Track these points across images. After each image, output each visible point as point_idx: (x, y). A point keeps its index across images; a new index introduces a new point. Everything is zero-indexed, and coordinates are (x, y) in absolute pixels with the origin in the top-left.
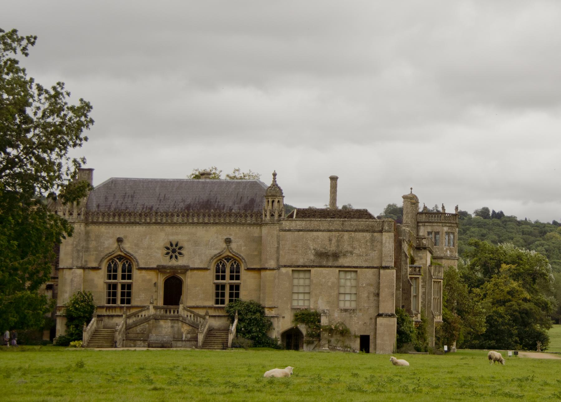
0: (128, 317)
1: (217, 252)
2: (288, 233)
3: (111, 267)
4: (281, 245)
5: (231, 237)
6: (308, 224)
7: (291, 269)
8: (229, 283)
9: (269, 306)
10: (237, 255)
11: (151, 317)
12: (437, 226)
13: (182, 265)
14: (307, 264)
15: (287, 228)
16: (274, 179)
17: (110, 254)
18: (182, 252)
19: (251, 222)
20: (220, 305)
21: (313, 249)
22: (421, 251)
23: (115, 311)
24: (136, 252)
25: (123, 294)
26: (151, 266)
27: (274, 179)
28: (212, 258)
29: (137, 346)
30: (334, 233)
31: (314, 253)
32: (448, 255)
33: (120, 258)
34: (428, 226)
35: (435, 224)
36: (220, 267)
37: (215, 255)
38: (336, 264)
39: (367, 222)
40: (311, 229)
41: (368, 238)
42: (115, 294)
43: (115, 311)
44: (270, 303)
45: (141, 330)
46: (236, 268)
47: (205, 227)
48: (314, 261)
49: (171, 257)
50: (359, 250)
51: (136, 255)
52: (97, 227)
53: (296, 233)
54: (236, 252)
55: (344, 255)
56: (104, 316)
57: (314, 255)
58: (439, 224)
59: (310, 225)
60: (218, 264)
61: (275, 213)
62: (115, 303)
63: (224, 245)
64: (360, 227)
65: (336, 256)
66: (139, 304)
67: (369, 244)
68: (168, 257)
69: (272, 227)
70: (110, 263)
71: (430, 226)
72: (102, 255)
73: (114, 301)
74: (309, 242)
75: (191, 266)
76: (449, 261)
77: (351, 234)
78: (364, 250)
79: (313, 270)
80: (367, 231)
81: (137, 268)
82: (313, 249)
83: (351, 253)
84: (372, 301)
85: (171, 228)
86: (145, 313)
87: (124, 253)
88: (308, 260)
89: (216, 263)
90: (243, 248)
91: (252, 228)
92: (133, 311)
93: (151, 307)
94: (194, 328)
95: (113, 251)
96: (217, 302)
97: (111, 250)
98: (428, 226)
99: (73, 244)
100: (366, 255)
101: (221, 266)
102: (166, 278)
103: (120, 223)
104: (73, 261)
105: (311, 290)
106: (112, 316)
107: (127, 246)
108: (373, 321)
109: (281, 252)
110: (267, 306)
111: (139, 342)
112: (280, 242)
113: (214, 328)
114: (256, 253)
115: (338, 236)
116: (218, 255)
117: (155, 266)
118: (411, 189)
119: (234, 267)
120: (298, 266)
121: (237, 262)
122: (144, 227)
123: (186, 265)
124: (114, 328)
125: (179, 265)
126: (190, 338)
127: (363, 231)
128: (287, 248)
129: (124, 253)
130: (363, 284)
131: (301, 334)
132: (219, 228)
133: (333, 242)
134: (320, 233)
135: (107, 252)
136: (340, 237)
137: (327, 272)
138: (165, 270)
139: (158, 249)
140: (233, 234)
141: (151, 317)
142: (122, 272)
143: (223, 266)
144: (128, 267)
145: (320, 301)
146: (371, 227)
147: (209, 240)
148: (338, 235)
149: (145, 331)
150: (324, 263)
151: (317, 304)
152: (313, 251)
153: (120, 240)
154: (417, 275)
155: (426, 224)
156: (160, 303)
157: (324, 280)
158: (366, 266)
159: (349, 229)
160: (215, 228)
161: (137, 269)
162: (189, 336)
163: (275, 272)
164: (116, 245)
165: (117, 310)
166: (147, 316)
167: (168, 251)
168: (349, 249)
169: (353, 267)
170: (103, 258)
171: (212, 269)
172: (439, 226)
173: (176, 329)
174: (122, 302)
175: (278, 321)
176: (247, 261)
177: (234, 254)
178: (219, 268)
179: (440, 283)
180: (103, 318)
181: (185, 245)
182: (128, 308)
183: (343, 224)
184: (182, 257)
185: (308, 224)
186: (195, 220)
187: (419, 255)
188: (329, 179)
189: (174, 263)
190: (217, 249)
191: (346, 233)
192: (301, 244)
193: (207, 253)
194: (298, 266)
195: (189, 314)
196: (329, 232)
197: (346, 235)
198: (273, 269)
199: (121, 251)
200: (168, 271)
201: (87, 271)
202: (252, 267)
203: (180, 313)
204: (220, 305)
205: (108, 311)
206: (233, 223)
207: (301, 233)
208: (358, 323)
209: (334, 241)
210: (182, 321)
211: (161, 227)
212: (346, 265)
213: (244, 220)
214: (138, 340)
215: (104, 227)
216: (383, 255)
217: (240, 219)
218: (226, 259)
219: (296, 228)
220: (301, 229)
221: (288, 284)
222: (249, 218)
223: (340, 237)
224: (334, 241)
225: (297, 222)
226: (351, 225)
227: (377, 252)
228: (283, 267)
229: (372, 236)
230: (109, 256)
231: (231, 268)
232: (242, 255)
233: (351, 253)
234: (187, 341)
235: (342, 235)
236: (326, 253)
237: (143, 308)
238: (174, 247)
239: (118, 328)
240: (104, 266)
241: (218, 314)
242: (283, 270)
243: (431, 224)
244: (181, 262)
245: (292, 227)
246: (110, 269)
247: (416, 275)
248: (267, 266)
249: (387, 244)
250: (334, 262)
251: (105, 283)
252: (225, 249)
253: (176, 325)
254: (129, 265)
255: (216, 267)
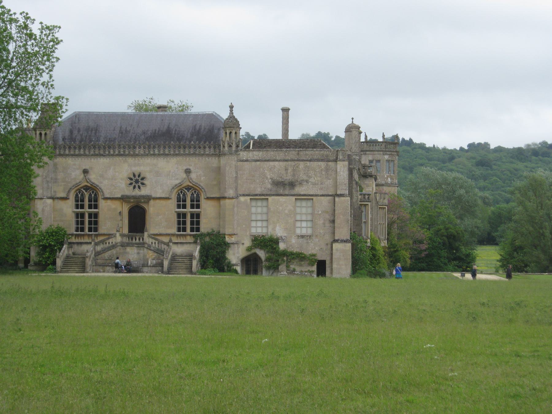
0: (97, 244)
1: (177, 182)
2: (246, 163)
3: (78, 197)
4: (239, 175)
5: (191, 168)
6: (265, 154)
7: (249, 198)
8: (190, 212)
9: (229, 233)
10: (197, 185)
11: (118, 244)
12: (378, 154)
13: (145, 195)
14: (264, 193)
15: (244, 159)
16: (231, 111)
17: (77, 185)
18: (145, 182)
19: (210, 153)
20: (181, 233)
21: (270, 178)
22: (367, 179)
23: (84, 238)
24: (101, 183)
25: (90, 223)
26: (116, 196)
27: (231, 111)
28: (173, 188)
29: (106, 271)
30: (290, 162)
31: (271, 182)
32: (389, 183)
33: (87, 188)
34: (369, 154)
35: (376, 153)
36: (180, 197)
37: (176, 185)
38: (293, 192)
39: (322, 152)
40: (267, 159)
41: (323, 167)
42: (83, 223)
43: (84, 238)
44: (230, 230)
45: (109, 256)
46: (196, 197)
47: (165, 159)
48: (271, 190)
49: (134, 187)
50: (315, 179)
51: (102, 186)
52: (64, 159)
53: (253, 163)
54: (196, 182)
55: (300, 184)
56: (74, 243)
57: (271, 184)
58: (379, 153)
59: (267, 155)
60: (179, 193)
61: (232, 144)
62: (185, 231)
63: (184, 176)
64: (315, 157)
65: (292, 185)
66: (105, 232)
67: (324, 173)
68: (132, 187)
69: (230, 157)
70: (77, 193)
71: (371, 154)
72: (70, 185)
73: (82, 230)
74: (266, 171)
75: (154, 196)
76: (390, 188)
77: (307, 163)
78: (319, 179)
79: (270, 198)
80: (322, 160)
81: (102, 197)
82: (270, 178)
83: (307, 181)
84: (328, 227)
85: (133, 159)
86: (112, 241)
87: (90, 184)
88: (265, 188)
89: (177, 192)
90: (202, 178)
91: (210, 158)
92: (100, 238)
93: (118, 234)
94: (159, 255)
95: (80, 182)
96: (179, 230)
97: (78, 181)
98: (369, 154)
99: (43, 176)
100: (322, 184)
101: (181, 196)
102: (131, 206)
103: (85, 155)
104: (43, 191)
105: (269, 217)
106: (81, 243)
107: (93, 177)
108: (329, 246)
109: (239, 182)
110: (227, 234)
111: (108, 268)
112: (238, 172)
113: (176, 255)
114: (215, 183)
115: (294, 166)
116: (178, 185)
117: (119, 196)
118: (353, 119)
119: (194, 197)
120: (256, 195)
121: (197, 192)
122: (108, 159)
123: (148, 194)
124: (85, 255)
125: (143, 195)
126: (155, 264)
127: (318, 160)
128: (245, 178)
129: (90, 184)
130: (319, 211)
131: (260, 258)
132: (179, 159)
133: (289, 171)
134: (277, 163)
135: (74, 183)
136: (296, 166)
137: (284, 200)
138: (129, 200)
139: (122, 179)
140: (193, 165)
141: (118, 244)
142: (89, 225)
143: (184, 195)
144: (94, 197)
145: (278, 228)
146: (326, 156)
147: (170, 171)
148: (294, 164)
149: (113, 257)
150: (281, 192)
151: (275, 230)
152: (270, 180)
153: (85, 172)
154: (367, 201)
155: (367, 153)
156: (126, 231)
157: (281, 208)
158: (321, 194)
159: (305, 159)
160: (175, 159)
161: (205, 199)
162: (154, 262)
163: (234, 200)
164: (82, 176)
165: (85, 237)
166: (114, 243)
167: (132, 181)
168: (305, 178)
169: (309, 195)
170: (70, 189)
171: (173, 199)
172: (380, 154)
173: (142, 255)
174: (90, 230)
175: (238, 248)
176: (206, 190)
177: (194, 184)
178: (180, 197)
179: (385, 209)
180: (73, 245)
181: (148, 175)
182: (97, 236)
183: (298, 154)
184: (144, 187)
185: (265, 154)
186: (156, 152)
187: (366, 182)
188: (281, 111)
189: (137, 192)
190: (177, 179)
191: (301, 162)
192: (258, 173)
193: (168, 183)
194: (256, 195)
195: (154, 241)
196: (286, 162)
197: (302, 165)
198: (232, 198)
199: (88, 182)
200: (132, 200)
201: (56, 201)
202: (212, 196)
203: (145, 241)
204: (181, 233)
205: (77, 238)
206: (192, 154)
207: (258, 163)
208: (315, 248)
209: (290, 170)
210: (147, 248)
211: (124, 159)
212: (302, 193)
213: (203, 151)
214: (107, 266)
215: (70, 159)
216: (338, 184)
217: (199, 151)
218: (84, 189)
219: (253, 158)
220: (258, 159)
221: (246, 212)
222: (207, 149)
223: (296, 166)
224: (290, 170)
225: (254, 152)
226: (306, 155)
227: (332, 180)
228: (241, 196)
229: (327, 165)
230: (76, 187)
231: (191, 197)
232: (202, 184)
233: (307, 181)
234: (153, 266)
235: (297, 165)
236: (282, 182)
237: (110, 236)
238: (137, 177)
239: (88, 254)
240: (72, 196)
241: (180, 241)
242: (242, 199)
243: (372, 153)
244: (144, 192)
245: (250, 157)
246: (77, 199)
247: (365, 202)
248: (226, 195)
249: (342, 173)
250: (291, 191)
251: (73, 212)
252: (185, 179)
253: (141, 251)
254: (95, 195)
255: (177, 197)
